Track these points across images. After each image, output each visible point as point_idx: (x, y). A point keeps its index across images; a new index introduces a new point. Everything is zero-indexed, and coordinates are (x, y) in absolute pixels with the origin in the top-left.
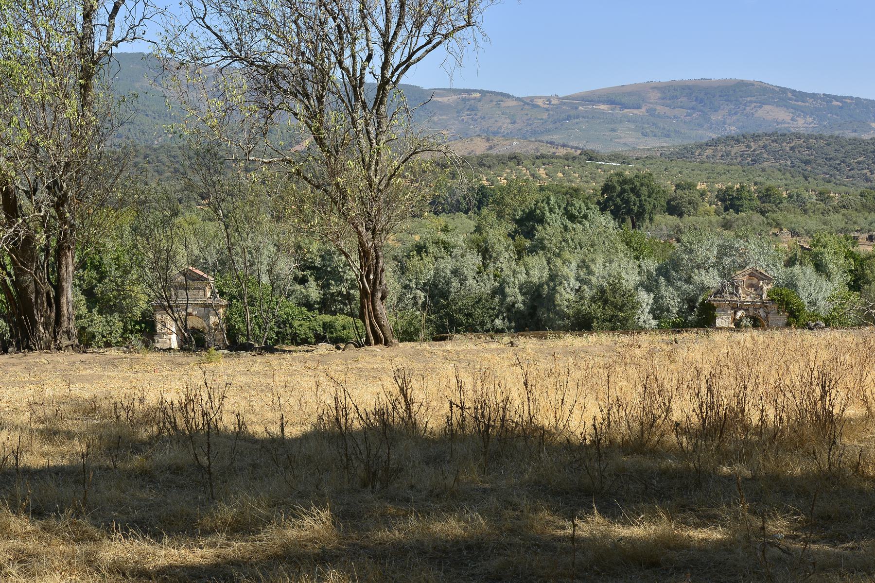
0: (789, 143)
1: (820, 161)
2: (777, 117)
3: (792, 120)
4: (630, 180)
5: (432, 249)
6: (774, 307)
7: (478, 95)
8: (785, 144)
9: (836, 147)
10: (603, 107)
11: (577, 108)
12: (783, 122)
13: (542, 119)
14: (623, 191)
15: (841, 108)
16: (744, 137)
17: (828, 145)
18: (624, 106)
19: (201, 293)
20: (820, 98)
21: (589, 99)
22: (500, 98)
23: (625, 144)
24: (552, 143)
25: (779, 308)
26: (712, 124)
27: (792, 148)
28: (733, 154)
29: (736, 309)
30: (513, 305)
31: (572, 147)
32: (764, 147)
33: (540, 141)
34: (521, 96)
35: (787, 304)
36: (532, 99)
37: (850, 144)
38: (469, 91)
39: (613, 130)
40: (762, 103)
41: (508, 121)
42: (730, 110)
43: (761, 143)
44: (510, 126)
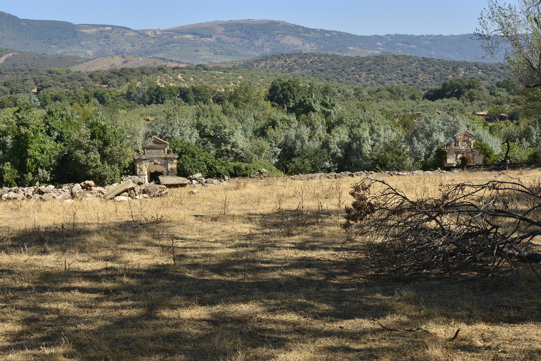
0: (309, 59)
1: (329, 70)
2: (294, 43)
3: (303, 45)
4: (287, 83)
6: (477, 152)
7: (110, 28)
8: (307, 60)
9: (337, 62)
10: (189, 36)
12: (297, 46)
13: (151, 44)
14: (283, 90)
15: (330, 37)
16: (282, 55)
17: (332, 60)
18: (202, 36)
19: (163, 151)
20: (318, 32)
21: (180, 31)
22: (124, 30)
23: (204, 60)
24: (163, 59)
25: (480, 152)
26: (255, 47)
27: (311, 62)
28: (277, 66)
29: (457, 153)
31: (176, 62)
32: (295, 61)
33: (156, 58)
36: (144, 31)
37: (345, 60)
38: (104, 26)
39: (197, 51)
40: (285, 35)
41: (130, 45)
42: (266, 39)
43: (293, 59)
44: (131, 48)
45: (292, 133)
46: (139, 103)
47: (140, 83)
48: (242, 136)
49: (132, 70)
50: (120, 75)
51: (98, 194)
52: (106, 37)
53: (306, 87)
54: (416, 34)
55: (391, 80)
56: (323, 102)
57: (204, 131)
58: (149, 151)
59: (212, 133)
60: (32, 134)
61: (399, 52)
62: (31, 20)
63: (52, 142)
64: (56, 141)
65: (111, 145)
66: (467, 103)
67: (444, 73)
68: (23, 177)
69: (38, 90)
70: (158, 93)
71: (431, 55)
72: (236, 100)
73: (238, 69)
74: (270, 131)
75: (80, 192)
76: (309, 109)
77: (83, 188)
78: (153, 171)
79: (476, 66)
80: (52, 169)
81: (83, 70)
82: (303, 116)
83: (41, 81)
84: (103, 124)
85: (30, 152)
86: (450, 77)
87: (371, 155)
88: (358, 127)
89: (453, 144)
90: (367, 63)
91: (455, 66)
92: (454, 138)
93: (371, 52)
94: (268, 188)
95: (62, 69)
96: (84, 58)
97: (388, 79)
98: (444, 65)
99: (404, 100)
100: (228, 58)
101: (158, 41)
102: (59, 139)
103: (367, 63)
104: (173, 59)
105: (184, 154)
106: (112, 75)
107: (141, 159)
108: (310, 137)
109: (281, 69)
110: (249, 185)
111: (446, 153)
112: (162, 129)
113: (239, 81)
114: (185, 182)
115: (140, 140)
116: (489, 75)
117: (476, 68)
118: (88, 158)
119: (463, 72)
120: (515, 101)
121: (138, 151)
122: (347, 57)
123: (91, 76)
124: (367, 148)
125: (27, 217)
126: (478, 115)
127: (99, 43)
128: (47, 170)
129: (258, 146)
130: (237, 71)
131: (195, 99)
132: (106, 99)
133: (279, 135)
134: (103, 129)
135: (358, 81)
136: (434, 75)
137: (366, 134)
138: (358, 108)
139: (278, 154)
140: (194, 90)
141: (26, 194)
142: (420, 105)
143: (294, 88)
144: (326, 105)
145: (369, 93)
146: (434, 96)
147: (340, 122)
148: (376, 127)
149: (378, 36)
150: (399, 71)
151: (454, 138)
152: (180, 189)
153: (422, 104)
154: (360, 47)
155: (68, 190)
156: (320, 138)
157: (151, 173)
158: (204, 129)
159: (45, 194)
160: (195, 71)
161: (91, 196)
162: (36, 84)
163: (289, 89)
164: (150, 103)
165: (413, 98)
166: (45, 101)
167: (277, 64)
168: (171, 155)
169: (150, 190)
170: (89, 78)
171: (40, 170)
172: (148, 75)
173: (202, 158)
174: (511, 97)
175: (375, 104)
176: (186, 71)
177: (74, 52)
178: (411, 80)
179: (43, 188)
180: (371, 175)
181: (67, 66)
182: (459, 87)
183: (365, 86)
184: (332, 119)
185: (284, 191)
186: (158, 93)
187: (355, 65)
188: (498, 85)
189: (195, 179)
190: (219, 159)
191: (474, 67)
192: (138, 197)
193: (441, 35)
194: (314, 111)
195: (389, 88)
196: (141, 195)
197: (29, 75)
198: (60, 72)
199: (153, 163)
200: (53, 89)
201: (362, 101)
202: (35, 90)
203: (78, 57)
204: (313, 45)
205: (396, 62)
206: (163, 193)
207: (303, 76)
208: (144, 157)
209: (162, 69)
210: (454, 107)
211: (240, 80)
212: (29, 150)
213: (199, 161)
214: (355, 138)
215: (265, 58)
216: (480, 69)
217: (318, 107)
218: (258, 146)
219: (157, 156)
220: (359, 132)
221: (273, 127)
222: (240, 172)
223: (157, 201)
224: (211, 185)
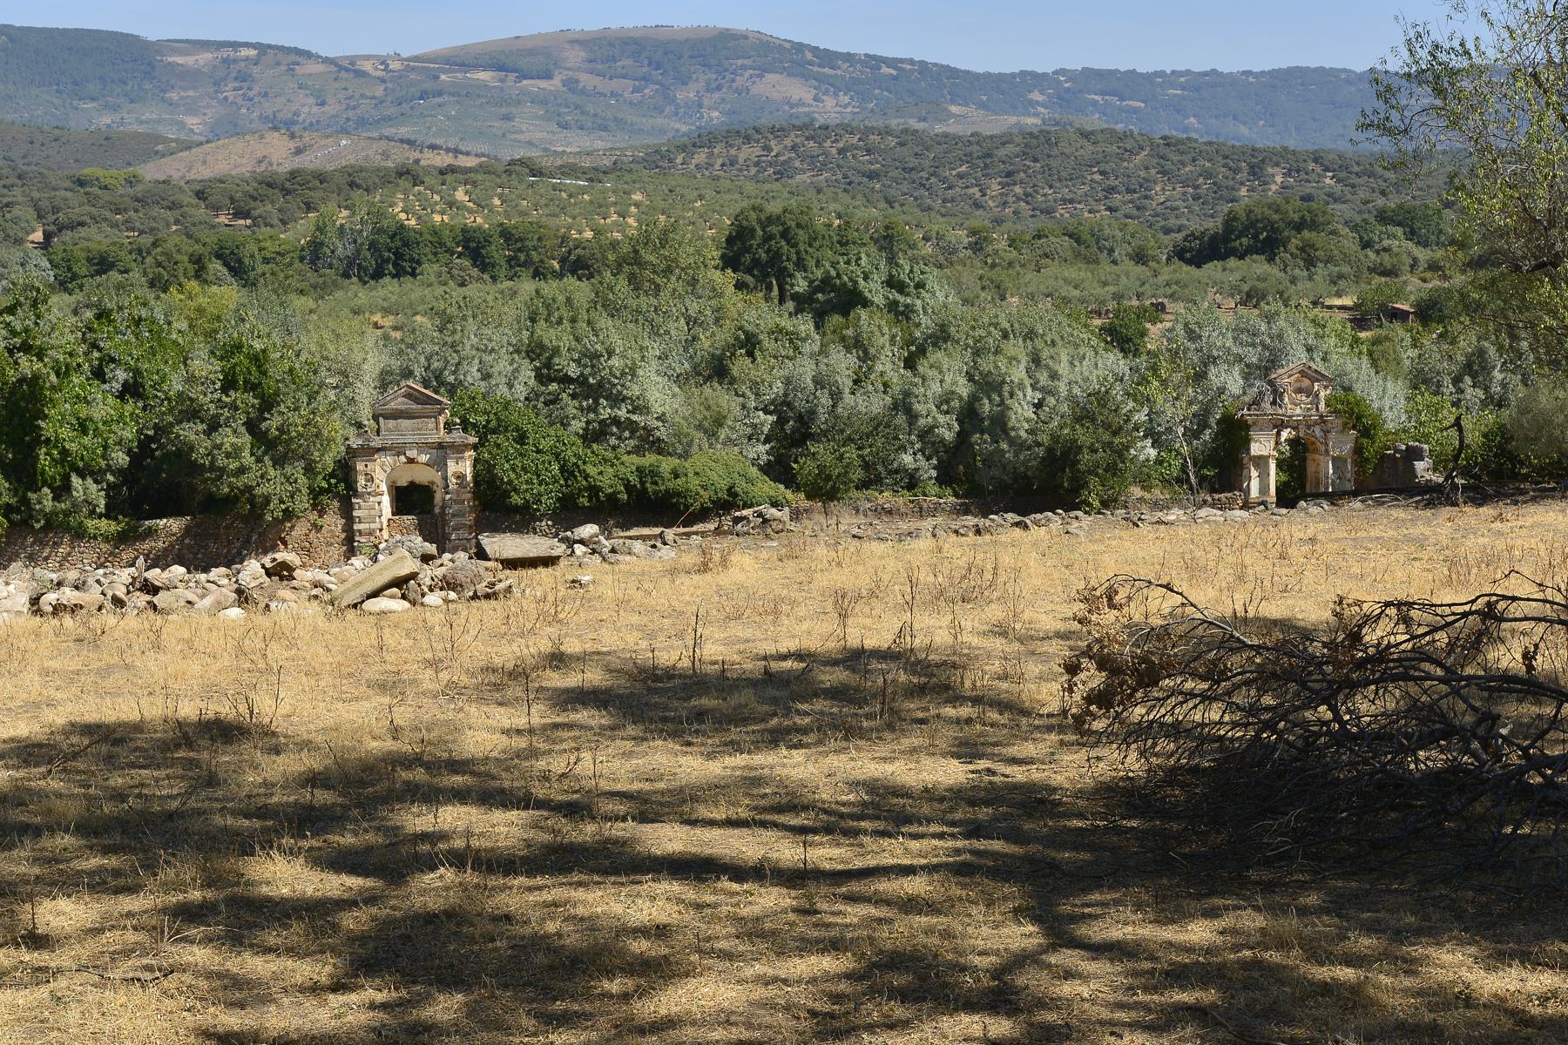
2: (787, 92)
3: (816, 99)
4: (778, 218)
5: (768, 343)
7: (253, 52)
8: (828, 144)
9: (917, 149)
10: (483, 76)
11: (437, 78)
12: (801, 103)
13: (374, 97)
14: (768, 238)
15: (896, 78)
16: (757, 131)
17: (902, 144)
19: (431, 423)
21: (459, 60)
22: (293, 58)
23: (530, 143)
24: (410, 143)
25: (1345, 424)
26: (678, 107)
27: (841, 151)
28: (741, 161)
29: (1280, 426)
30: (931, 429)
31: (448, 150)
32: (794, 148)
33: (389, 139)
34: (331, 55)
35: (1359, 418)
36: (353, 60)
37: (939, 143)
38: (235, 45)
39: (507, 118)
40: (764, 70)
41: (312, 100)
42: (708, 83)
43: (788, 142)
44: (315, 109)
45: (805, 370)
46: (346, 275)
47: (345, 213)
48: (659, 379)
49: (321, 177)
50: (286, 192)
51: (315, 592)
52: (243, 78)
53: (830, 225)
54: (1143, 68)
55: (1071, 201)
56: (891, 276)
57: (548, 365)
58: (392, 423)
59: (573, 371)
60: (53, 378)
61: (1094, 122)
62: (20, 29)
63: (110, 400)
64: (121, 396)
65: (282, 408)
66: (1297, 271)
67: (1225, 183)
68: (25, 501)
69: (48, 236)
70: (399, 244)
71: (1186, 130)
72: (639, 266)
73: (630, 171)
74: (740, 366)
75: (260, 586)
76: (850, 300)
77: (269, 573)
78: (403, 483)
79: (1316, 161)
80: (110, 478)
81: (176, 176)
82: (836, 319)
83: (56, 210)
84: (258, 345)
85: (47, 428)
86: (1243, 192)
87: (1031, 432)
88: (996, 353)
89: (1269, 398)
90: (1002, 152)
91: (1257, 164)
92: (1271, 383)
93: (1013, 120)
94: (791, 565)
95: (113, 172)
96: (176, 141)
97: (1065, 201)
98: (1226, 157)
99: (1115, 262)
100: (600, 138)
101: (393, 90)
102: (132, 390)
103: (1002, 152)
104: (438, 142)
105: (494, 431)
106: (264, 190)
107: (369, 448)
108: (856, 382)
109: (753, 170)
110: (735, 558)
111: (1248, 427)
112: (428, 359)
113: (633, 209)
114: (555, 553)
115: (366, 393)
116: (1353, 186)
117: (1319, 169)
118: (219, 447)
119: (1279, 179)
120: (1434, 267)
121: (359, 425)
122: (946, 135)
123: (200, 195)
124: (1021, 413)
125: (127, 667)
126: (1330, 307)
127: (221, 96)
128: (96, 482)
129: (708, 408)
130: (628, 177)
131: (508, 262)
132: (246, 261)
133: (770, 376)
134: (259, 359)
135: (977, 205)
136: (1196, 187)
137: (1018, 373)
138: (983, 288)
139: (766, 429)
140: (506, 234)
141: (109, 594)
142: (1162, 279)
143: (801, 232)
144: (901, 287)
145: (1012, 243)
146: (1203, 251)
147: (941, 337)
148: (1045, 354)
149: (1033, 75)
150: (1097, 177)
151: (1271, 383)
152: (543, 572)
153: (1166, 277)
154: (982, 106)
155: (226, 581)
156: (885, 385)
157: (398, 488)
158: (550, 358)
159: (161, 594)
160: (505, 178)
161: (294, 597)
162: (40, 217)
163: (785, 234)
164: (378, 275)
165: (1140, 257)
166: (70, 269)
167: (742, 157)
168: (457, 436)
169: (461, 577)
170: (195, 201)
171: (76, 480)
172: (367, 190)
173: (544, 444)
174: (1423, 255)
175: (1030, 275)
176: (480, 177)
177: (147, 122)
178: (1131, 202)
179: (155, 575)
180: (1075, 524)
181: (129, 164)
182: (1272, 227)
183: (998, 221)
184: (918, 325)
185: (843, 578)
186: (399, 244)
187: (968, 158)
188: (1383, 217)
189: (582, 542)
190: (595, 446)
191: (1311, 166)
192: (427, 600)
193: (1214, 71)
194: (866, 303)
195: (1071, 228)
196: (438, 593)
197: (17, 191)
198: (108, 181)
199: (403, 459)
200: (91, 232)
201: (993, 266)
202: (38, 236)
203: (160, 137)
204: (846, 99)
205: (1087, 151)
206: (499, 587)
207: (819, 191)
208: (376, 442)
209: (408, 172)
210: (1261, 285)
211: (637, 205)
212: (42, 424)
213: (538, 451)
214: (988, 385)
215: (706, 139)
216: (1327, 169)
217: (875, 291)
218: (708, 408)
219: (417, 439)
220: (997, 367)
221: (750, 354)
222: (656, 483)
223: (490, 611)
224: (628, 558)
